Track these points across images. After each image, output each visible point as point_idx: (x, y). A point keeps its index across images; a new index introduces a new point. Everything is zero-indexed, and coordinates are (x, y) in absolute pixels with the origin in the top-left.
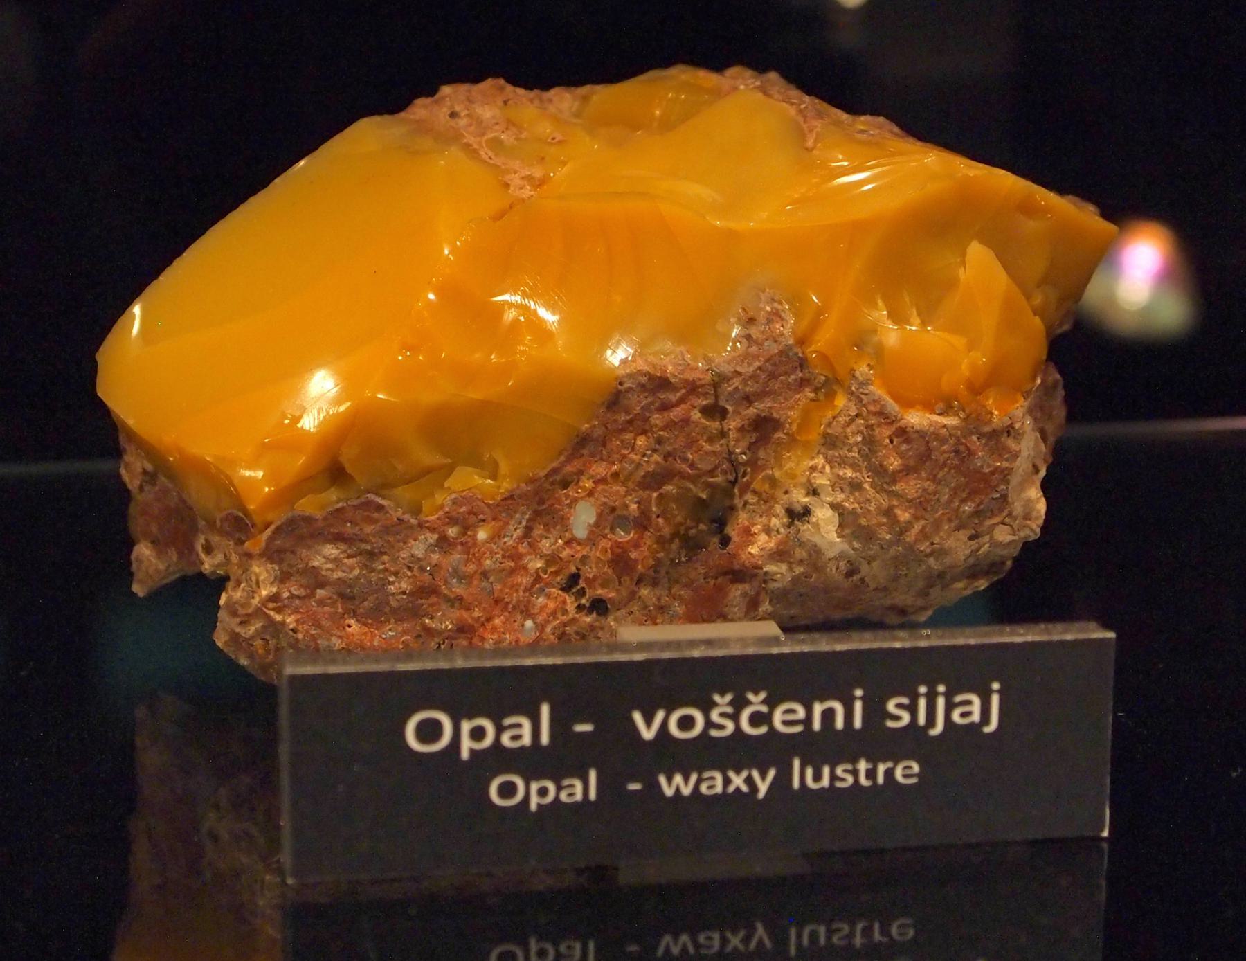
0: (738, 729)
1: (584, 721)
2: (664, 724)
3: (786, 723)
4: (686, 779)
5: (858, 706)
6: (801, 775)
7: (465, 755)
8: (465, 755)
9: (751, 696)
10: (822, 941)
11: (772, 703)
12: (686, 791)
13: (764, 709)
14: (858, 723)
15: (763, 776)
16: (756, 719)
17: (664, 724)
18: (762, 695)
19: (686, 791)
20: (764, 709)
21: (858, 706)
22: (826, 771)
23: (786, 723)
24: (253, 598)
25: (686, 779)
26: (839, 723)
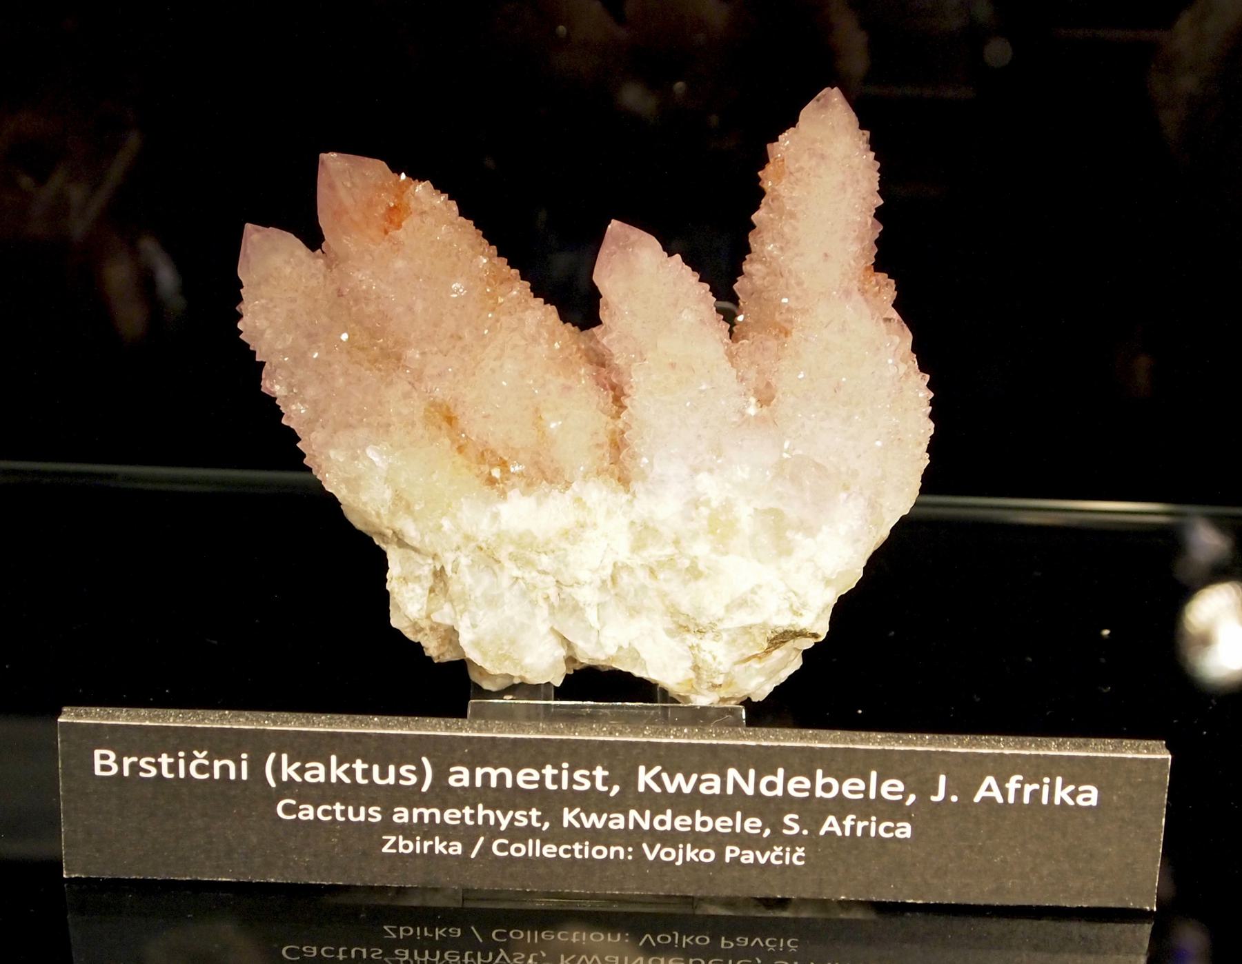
0: (841, 784)
1: (1176, 723)
3: (851, 792)
4: (599, 818)
5: (244, 765)
6: (731, 852)
7: (781, 771)
8: (781, 771)
9: (196, 753)
11: (210, 758)
12: (599, 825)
13: (206, 762)
14: (244, 777)
15: (505, 815)
16: (201, 769)
18: (205, 753)
19: (599, 825)
20: (206, 762)
21: (244, 765)
23: (851, 792)
24: (474, 374)
25: (599, 818)
26: (232, 776)
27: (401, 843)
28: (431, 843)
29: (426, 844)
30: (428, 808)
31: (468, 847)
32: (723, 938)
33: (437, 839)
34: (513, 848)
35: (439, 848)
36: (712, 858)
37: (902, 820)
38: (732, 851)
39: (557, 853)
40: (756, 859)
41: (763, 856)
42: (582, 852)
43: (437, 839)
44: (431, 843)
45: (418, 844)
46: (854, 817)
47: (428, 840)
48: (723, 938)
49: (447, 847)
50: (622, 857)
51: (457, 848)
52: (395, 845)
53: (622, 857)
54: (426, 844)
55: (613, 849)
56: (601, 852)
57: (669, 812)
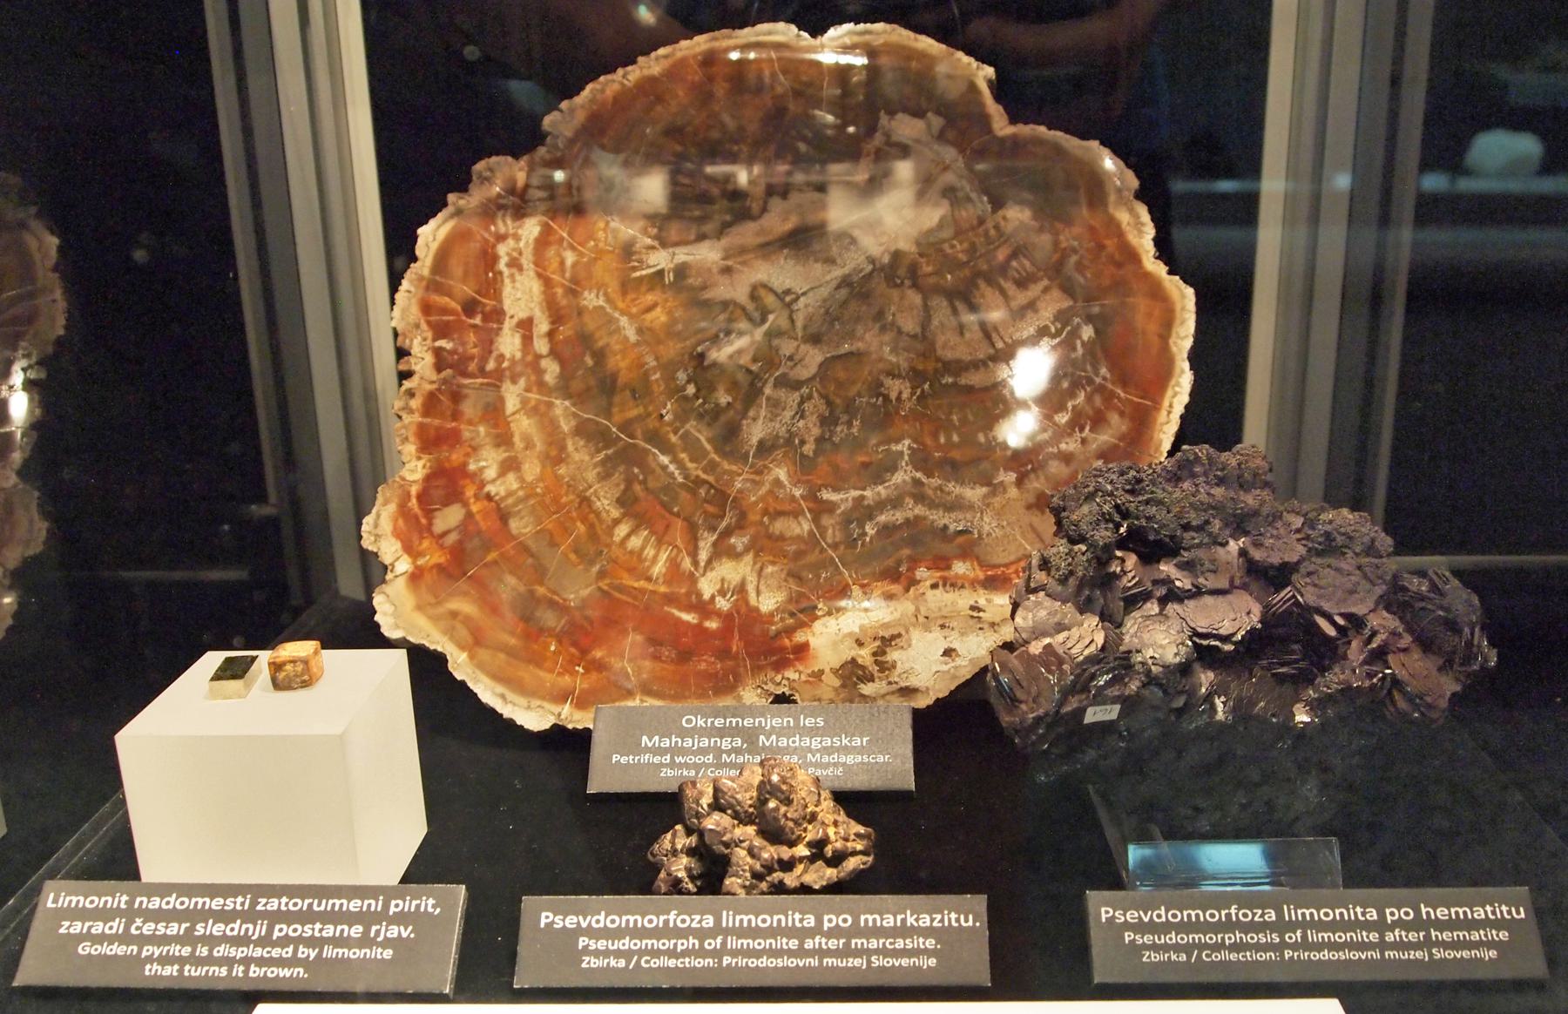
2: (1152, 916)
8: (1163, 908)
10: (879, 924)
14: (1285, 907)
17: (1152, 916)
22: (1191, 941)
27: (1153, 955)
28: (903, 916)
29: (1166, 955)
30: (1194, 910)
31: (1189, 956)
32: (1422, 906)
33: (908, 912)
34: (652, 962)
35: (1174, 957)
36: (1287, 936)
37: (808, 913)
38: (547, 917)
39: (224, 931)
40: (399, 933)
41: (585, 920)
42: (1251, 956)
43: (908, 912)
44: (903, 916)
45: (407, 903)
46: (676, 912)
47: (900, 914)
48: (1422, 906)
49: (917, 920)
50: (711, 965)
51: (622, 963)
52: (1149, 957)
53: (711, 965)
54: (899, 917)
55: (776, 918)
56: (1262, 956)
57: (603, 913)
